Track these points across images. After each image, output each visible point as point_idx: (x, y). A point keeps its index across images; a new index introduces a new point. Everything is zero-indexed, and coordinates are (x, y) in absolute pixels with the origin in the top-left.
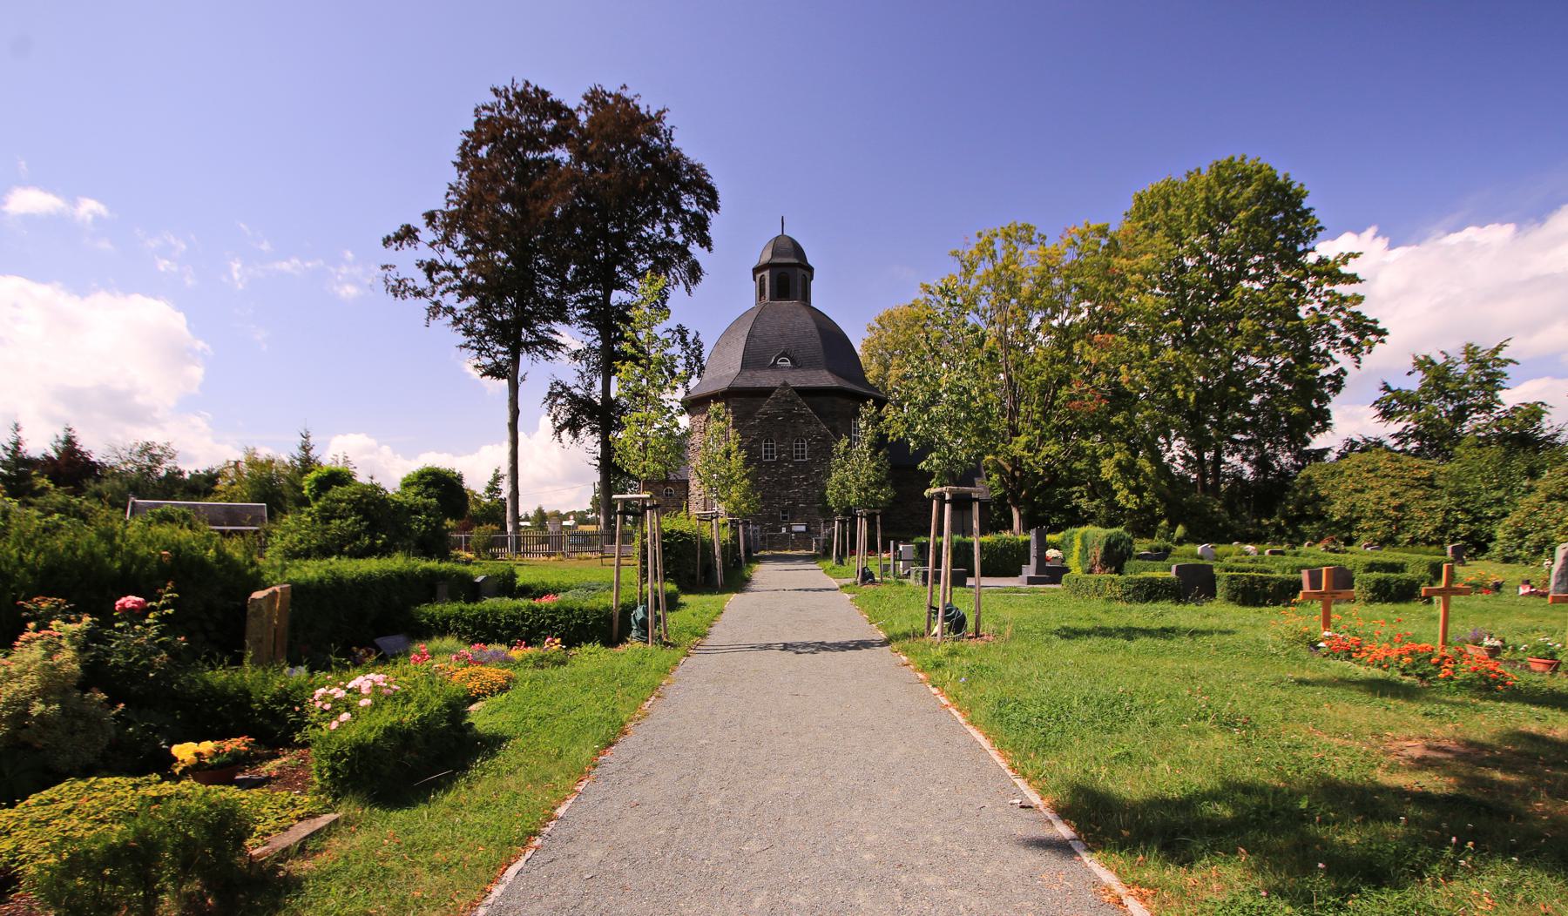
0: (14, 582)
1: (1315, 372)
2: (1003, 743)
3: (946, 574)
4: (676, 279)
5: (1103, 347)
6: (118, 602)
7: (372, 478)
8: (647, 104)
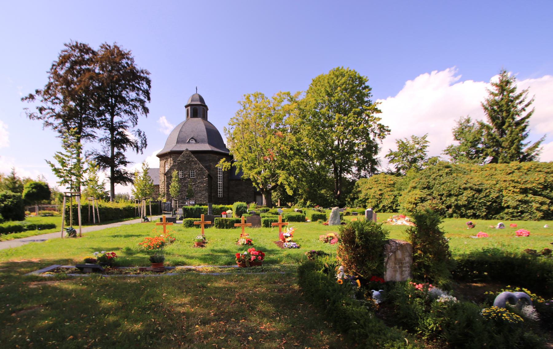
8: (124, 48)
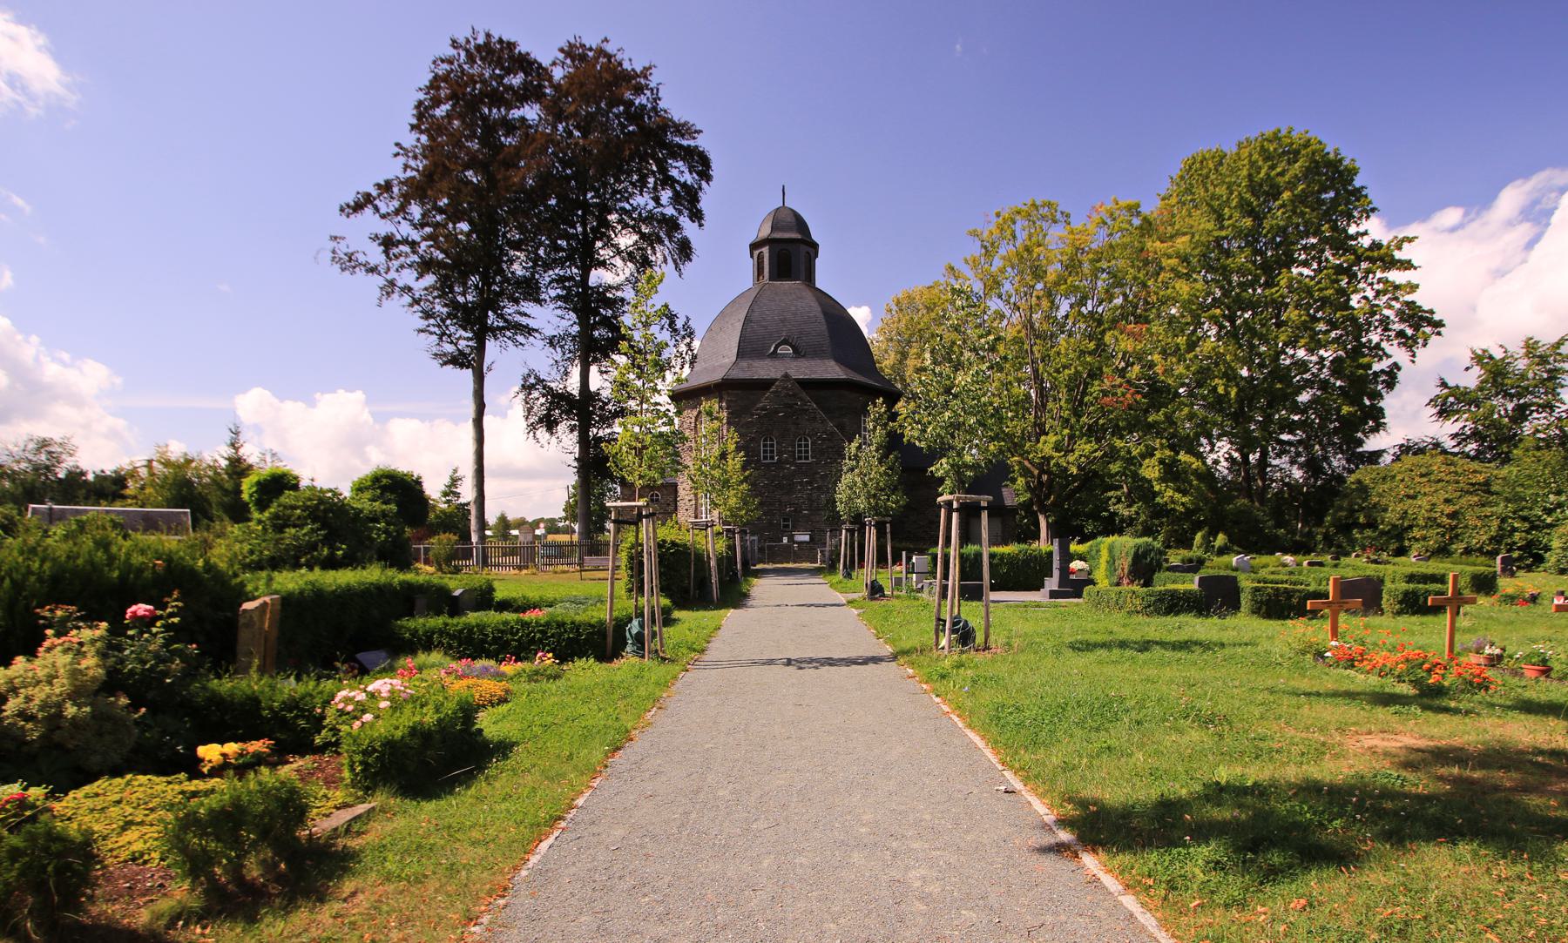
0: (25, 590)
1: (1369, 366)
2: (996, 742)
3: (954, 585)
4: (665, 257)
5: (1136, 337)
6: (129, 610)
7: (312, 480)
8: (633, 60)
